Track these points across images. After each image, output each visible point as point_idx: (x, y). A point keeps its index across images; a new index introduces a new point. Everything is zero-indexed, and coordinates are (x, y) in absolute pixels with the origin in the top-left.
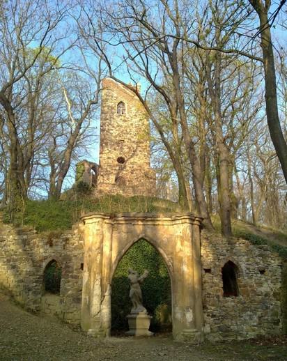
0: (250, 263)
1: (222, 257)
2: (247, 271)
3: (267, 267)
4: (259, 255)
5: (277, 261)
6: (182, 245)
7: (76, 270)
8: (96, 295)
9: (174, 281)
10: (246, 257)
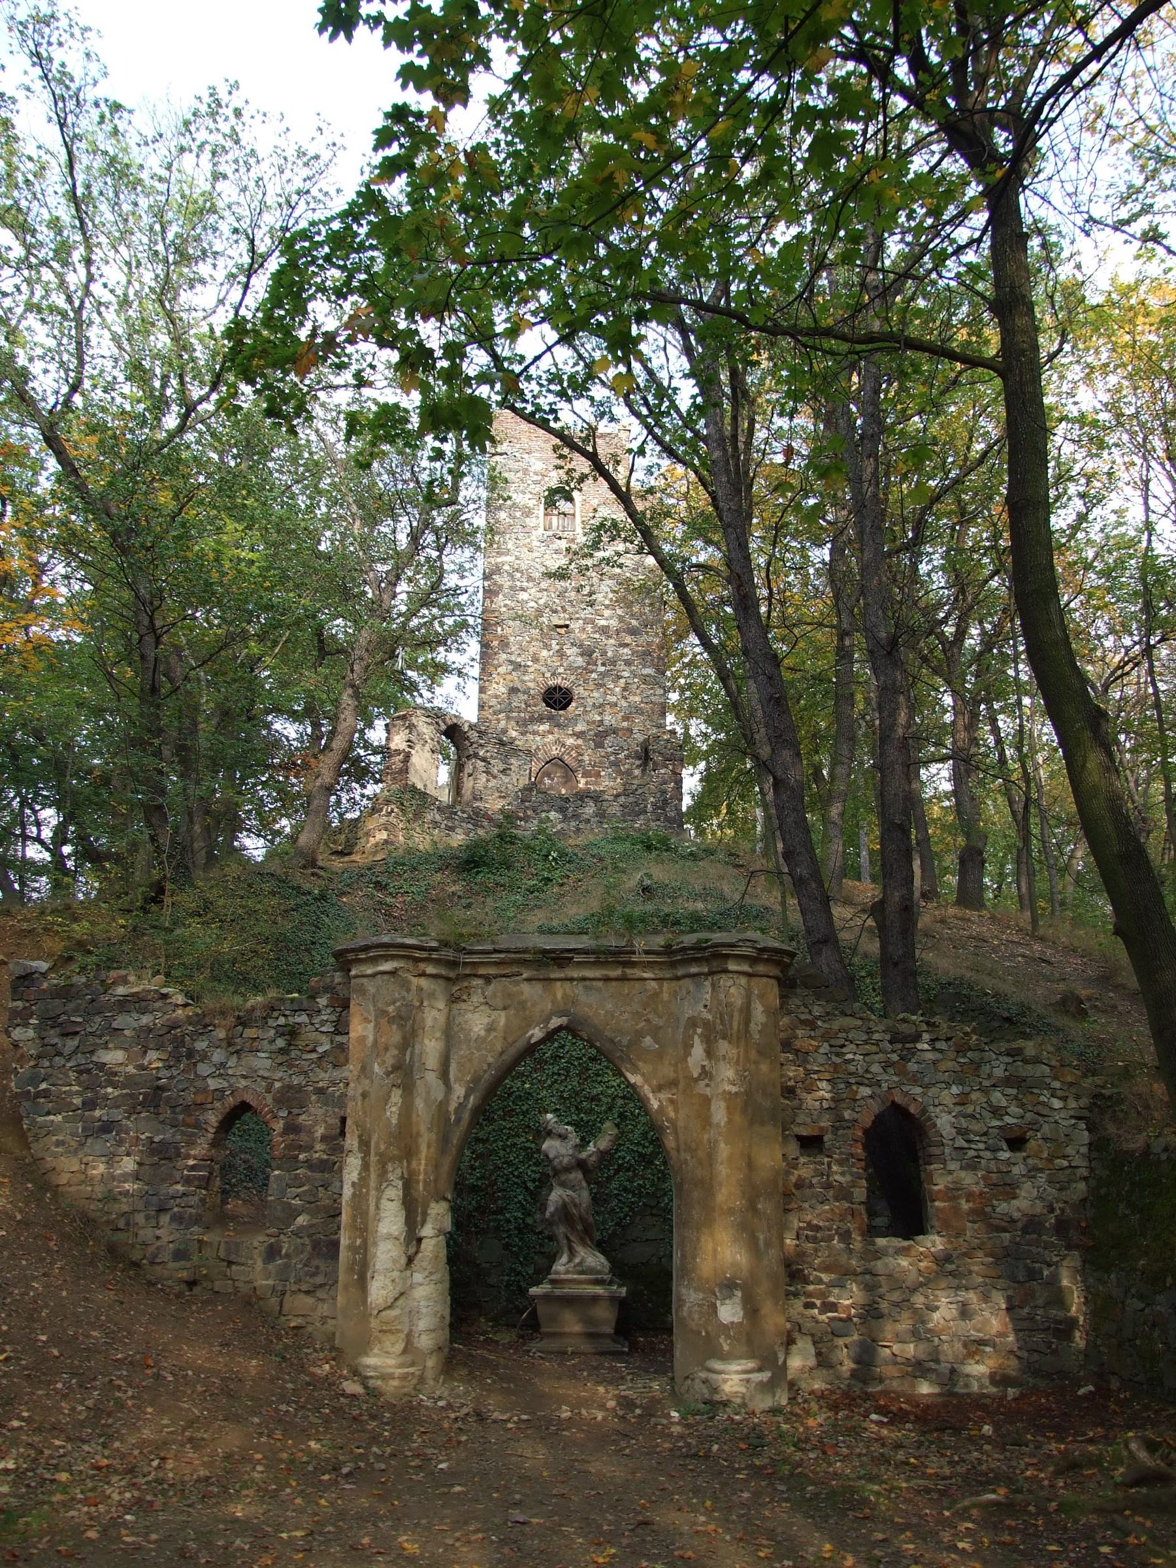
0: (970, 1109)
1: (865, 1091)
2: (960, 1142)
3: (1034, 1126)
4: (1008, 1081)
5: (1072, 1104)
6: (709, 1053)
7: (324, 1139)
8: (389, 1237)
9: (680, 1186)
10: (955, 1090)
